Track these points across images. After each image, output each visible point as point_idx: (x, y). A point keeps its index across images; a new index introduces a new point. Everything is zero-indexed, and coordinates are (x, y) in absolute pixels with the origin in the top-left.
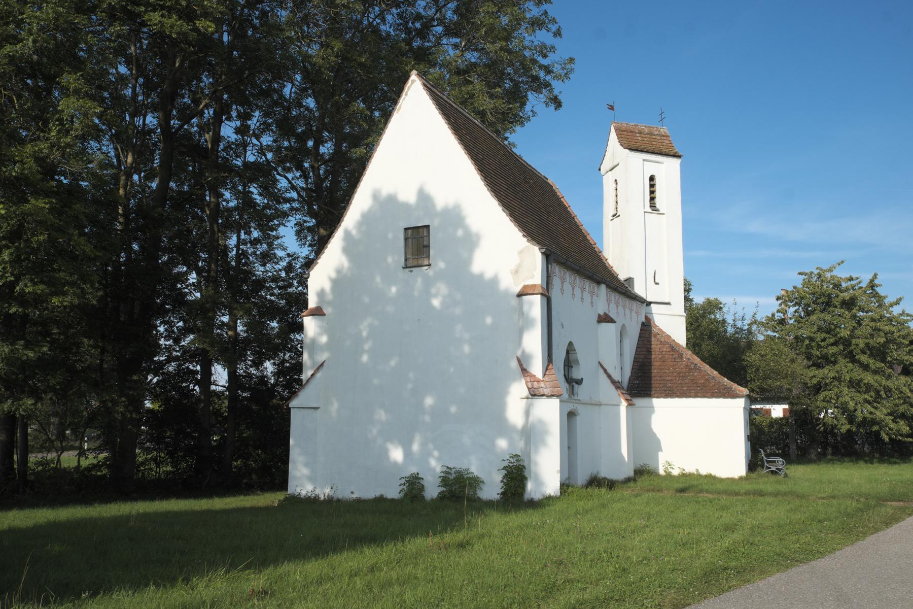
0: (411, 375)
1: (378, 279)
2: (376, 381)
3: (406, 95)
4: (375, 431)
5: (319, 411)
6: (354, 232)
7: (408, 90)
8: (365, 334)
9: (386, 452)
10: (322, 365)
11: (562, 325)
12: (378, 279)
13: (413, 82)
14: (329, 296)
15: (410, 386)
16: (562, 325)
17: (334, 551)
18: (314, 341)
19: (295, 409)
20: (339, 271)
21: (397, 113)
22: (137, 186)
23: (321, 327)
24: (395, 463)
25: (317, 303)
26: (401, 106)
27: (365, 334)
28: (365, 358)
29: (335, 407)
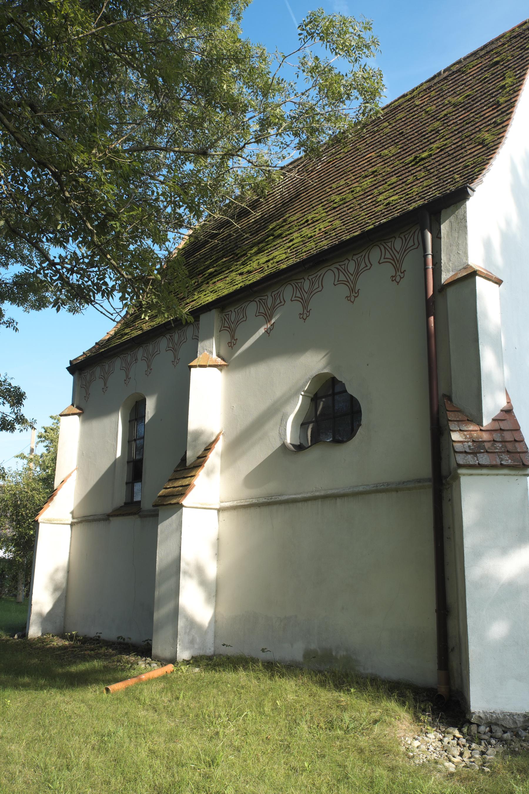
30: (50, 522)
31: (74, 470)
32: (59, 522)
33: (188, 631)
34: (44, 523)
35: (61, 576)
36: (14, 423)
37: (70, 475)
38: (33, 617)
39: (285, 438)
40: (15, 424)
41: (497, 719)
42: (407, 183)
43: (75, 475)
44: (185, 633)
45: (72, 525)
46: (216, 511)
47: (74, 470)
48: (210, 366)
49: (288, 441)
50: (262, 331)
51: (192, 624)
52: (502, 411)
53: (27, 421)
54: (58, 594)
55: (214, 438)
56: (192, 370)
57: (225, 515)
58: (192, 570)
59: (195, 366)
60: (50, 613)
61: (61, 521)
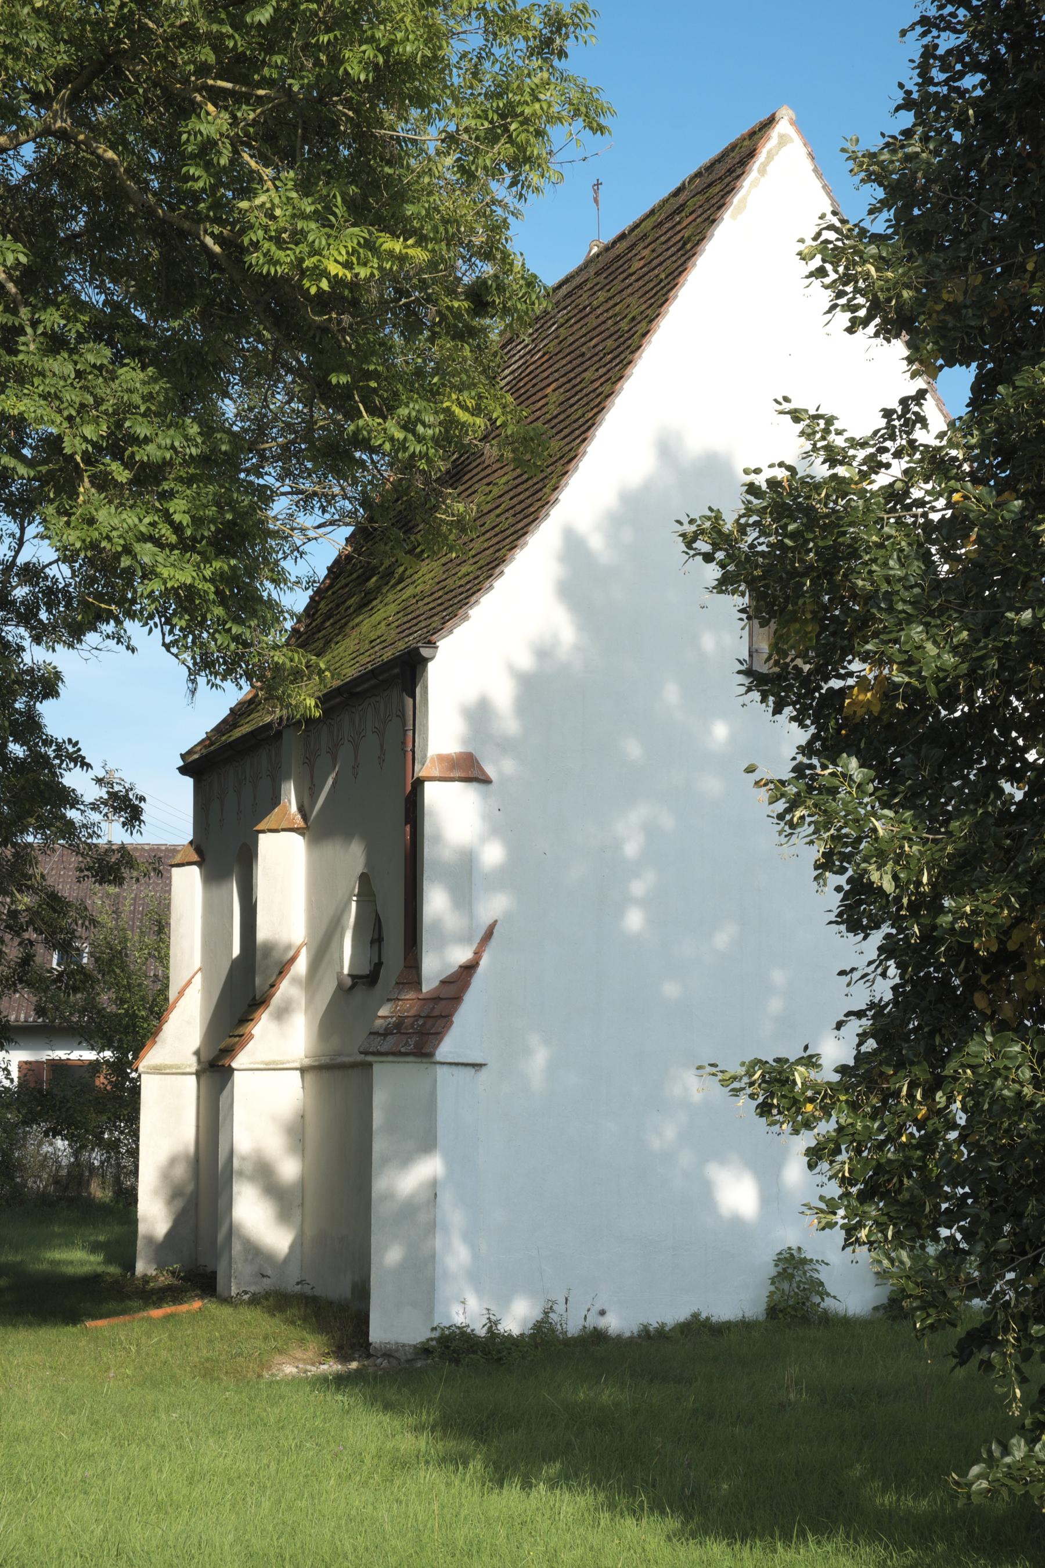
0: (778, 977)
1: (672, 693)
2: (671, 990)
3: (762, 171)
4: (670, 1133)
5: (484, 1073)
6: (596, 542)
7: (770, 157)
8: (631, 849)
9: (706, 1191)
10: (489, 935)
11: (567, 1300)
12: (672, 693)
13: (783, 140)
14: (509, 724)
15: (775, 1005)
16: (567, 1300)
17: (550, 1460)
18: (468, 860)
19: (445, 1068)
20: (543, 653)
21: (734, 217)
22: (945, 1135)
23: (486, 817)
24: (736, 1222)
25: (465, 742)
26: (744, 199)
27: (631, 849)
28: (634, 920)
29: (539, 1059)
30: (158, 1070)
31: (196, 973)
32: (174, 1071)
33: (250, 1257)
34: (148, 1073)
35: (180, 1171)
36: (119, 869)
37: (189, 983)
38: (140, 1243)
39: (342, 967)
40: (123, 870)
41: (390, 1350)
42: (459, 575)
43: (198, 980)
44: (246, 1260)
45: (198, 1074)
46: (298, 1073)
47: (196, 973)
48: (284, 830)
49: (346, 971)
50: (330, 781)
51: (255, 1251)
52: (461, 967)
53: (69, 904)
54: (179, 1204)
55: (291, 954)
56: (261, 836)
57: (308, 1077)
58: (248, 1168)
59: (263, 832)
60: (169, 1235)
61: (179, 1068)
